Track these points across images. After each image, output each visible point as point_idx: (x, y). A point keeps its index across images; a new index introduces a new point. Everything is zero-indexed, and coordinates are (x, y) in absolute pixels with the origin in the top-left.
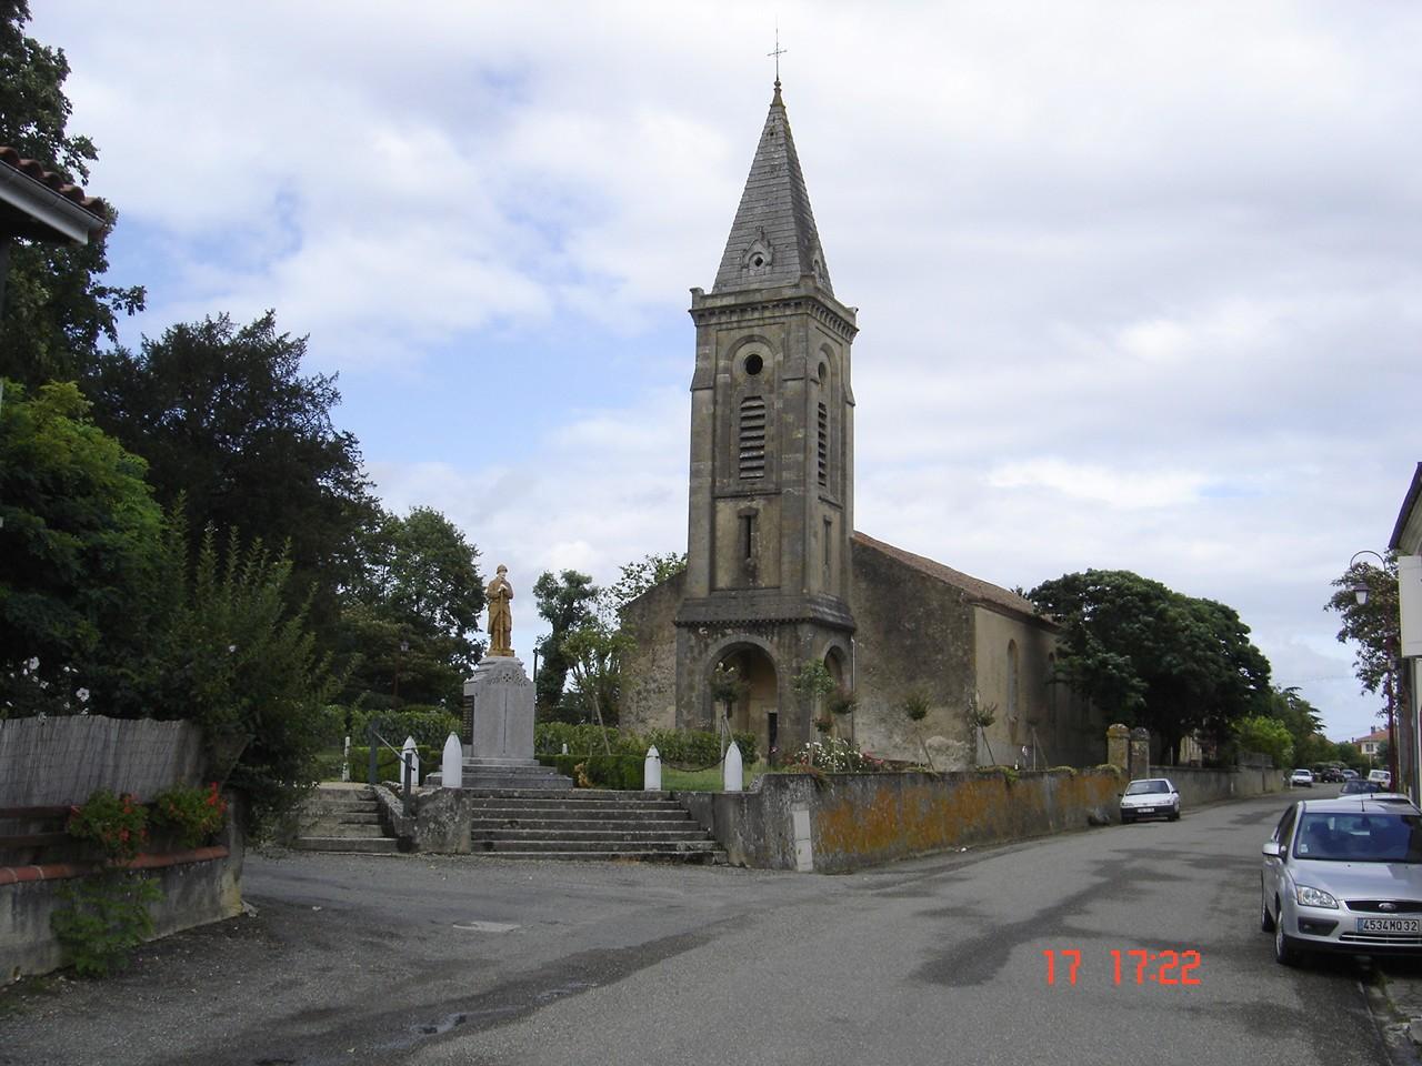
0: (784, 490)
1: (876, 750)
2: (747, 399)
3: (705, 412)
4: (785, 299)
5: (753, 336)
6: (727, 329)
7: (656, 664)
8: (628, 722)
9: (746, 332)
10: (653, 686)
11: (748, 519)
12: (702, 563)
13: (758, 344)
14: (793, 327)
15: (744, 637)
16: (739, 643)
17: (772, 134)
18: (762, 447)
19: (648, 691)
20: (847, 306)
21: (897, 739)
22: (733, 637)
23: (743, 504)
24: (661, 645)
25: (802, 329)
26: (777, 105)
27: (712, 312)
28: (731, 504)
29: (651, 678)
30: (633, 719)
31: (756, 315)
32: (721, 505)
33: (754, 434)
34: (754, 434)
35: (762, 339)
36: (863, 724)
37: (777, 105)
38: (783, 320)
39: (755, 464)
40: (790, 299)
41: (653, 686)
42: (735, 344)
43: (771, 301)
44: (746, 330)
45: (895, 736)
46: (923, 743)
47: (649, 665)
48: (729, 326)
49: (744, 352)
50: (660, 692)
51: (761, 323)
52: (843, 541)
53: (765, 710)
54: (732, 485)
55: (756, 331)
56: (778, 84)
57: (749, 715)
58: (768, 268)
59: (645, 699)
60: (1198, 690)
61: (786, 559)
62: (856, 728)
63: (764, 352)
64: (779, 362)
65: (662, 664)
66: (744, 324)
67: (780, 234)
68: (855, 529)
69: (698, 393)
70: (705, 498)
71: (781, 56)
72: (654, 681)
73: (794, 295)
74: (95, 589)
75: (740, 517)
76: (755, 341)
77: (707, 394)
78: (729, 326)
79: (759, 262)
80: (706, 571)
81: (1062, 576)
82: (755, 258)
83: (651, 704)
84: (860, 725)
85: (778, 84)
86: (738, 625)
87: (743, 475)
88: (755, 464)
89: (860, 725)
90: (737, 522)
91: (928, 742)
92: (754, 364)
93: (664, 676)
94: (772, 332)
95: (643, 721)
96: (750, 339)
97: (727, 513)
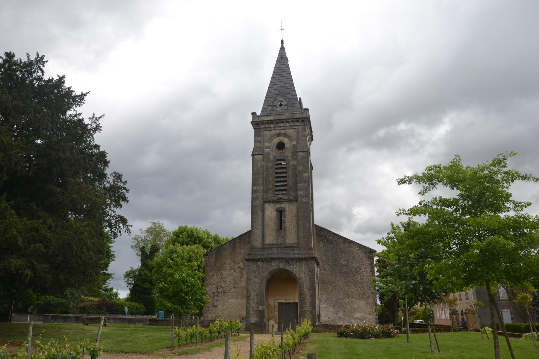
0: (299, 199)
1: (331, 320)
2: (278, 160)
3: (259, 164)
4: (297, 118)
5: (281, 133)
6: (269, 130)
7: (222, 279)
8: (208, 307)
9: (277, 132)
10: (221, 290)
11: (281, 213)
12: (258, 231)
13: (283, 138)
14: (300, 130)
15: (282, 265)
16: (279, 269)
17: (282, 58)
18: (286, 181)
19: (219, 292)
20: (252, 157)
21: (341, 315)
22: (275, 265)
23: (278, 206)
24: (225, 271)
25: (304, 131)
26: (282, 49)
27: (262, 123)
28: (272, 205)
29: (220, 286)
30: (210, 305)
31: (282, 125)
32: (267, 206)
33: (282, 175)
34: (282, 175)
35: (285, 135)
36: (324, 307)
37: (282, 49)
38: (295, 127)
39: (282, 188)
40: (299, 118)
41: (221, 290)
42: (272, 137)
43: (290, 119)
44: (278, 131)
45: (340, 313)
46: (353, 317)
47: (219, 280)
48: (270, 129)
49: (276, 140)
50: (224, 293)
51: (285, 128)
52: (313, 225)
53: (276, 301)
54: (270, 196)
55: (283, 131)
56: (282, 41)
57: (268, 303)
58: (285, 107)
59: (217, 296)
60: (421, 293)
61: (301, 230)
62: (321, 309)
63: (286, 140)
64: (294, 145)
65: (225, 280)
66: (277, 128)
67: (290, 95)
68: (316, 222)
69: (256, 156)
70: (259, 202)
71: (280, 28)
72: (222, 288)
73: (301, 117)
74: (67, 344)
75: (277, 211)
76: (281, 136)
77: (259, 157)
78: (270, 129)
79: (281, 105)
80: (261, 235)
81: (130, 269)
82: (279, 103)
83: (220, 298)
84: (323, 308)
85: (282, 41)
86: (279, 259)
87: (277, 193)
88: (282, 188)
89: (323, 308)
90: (275, 213)
91: (355, 316)
92: (281, 146)
93: (226, 285)
94: (291, 132)
95: (216, 306)
96: (279, 135)
97: (270, 212)
